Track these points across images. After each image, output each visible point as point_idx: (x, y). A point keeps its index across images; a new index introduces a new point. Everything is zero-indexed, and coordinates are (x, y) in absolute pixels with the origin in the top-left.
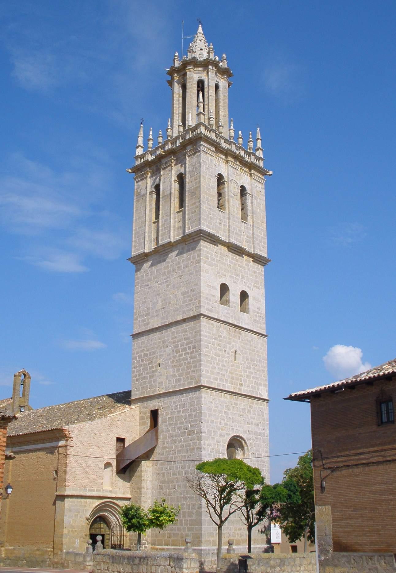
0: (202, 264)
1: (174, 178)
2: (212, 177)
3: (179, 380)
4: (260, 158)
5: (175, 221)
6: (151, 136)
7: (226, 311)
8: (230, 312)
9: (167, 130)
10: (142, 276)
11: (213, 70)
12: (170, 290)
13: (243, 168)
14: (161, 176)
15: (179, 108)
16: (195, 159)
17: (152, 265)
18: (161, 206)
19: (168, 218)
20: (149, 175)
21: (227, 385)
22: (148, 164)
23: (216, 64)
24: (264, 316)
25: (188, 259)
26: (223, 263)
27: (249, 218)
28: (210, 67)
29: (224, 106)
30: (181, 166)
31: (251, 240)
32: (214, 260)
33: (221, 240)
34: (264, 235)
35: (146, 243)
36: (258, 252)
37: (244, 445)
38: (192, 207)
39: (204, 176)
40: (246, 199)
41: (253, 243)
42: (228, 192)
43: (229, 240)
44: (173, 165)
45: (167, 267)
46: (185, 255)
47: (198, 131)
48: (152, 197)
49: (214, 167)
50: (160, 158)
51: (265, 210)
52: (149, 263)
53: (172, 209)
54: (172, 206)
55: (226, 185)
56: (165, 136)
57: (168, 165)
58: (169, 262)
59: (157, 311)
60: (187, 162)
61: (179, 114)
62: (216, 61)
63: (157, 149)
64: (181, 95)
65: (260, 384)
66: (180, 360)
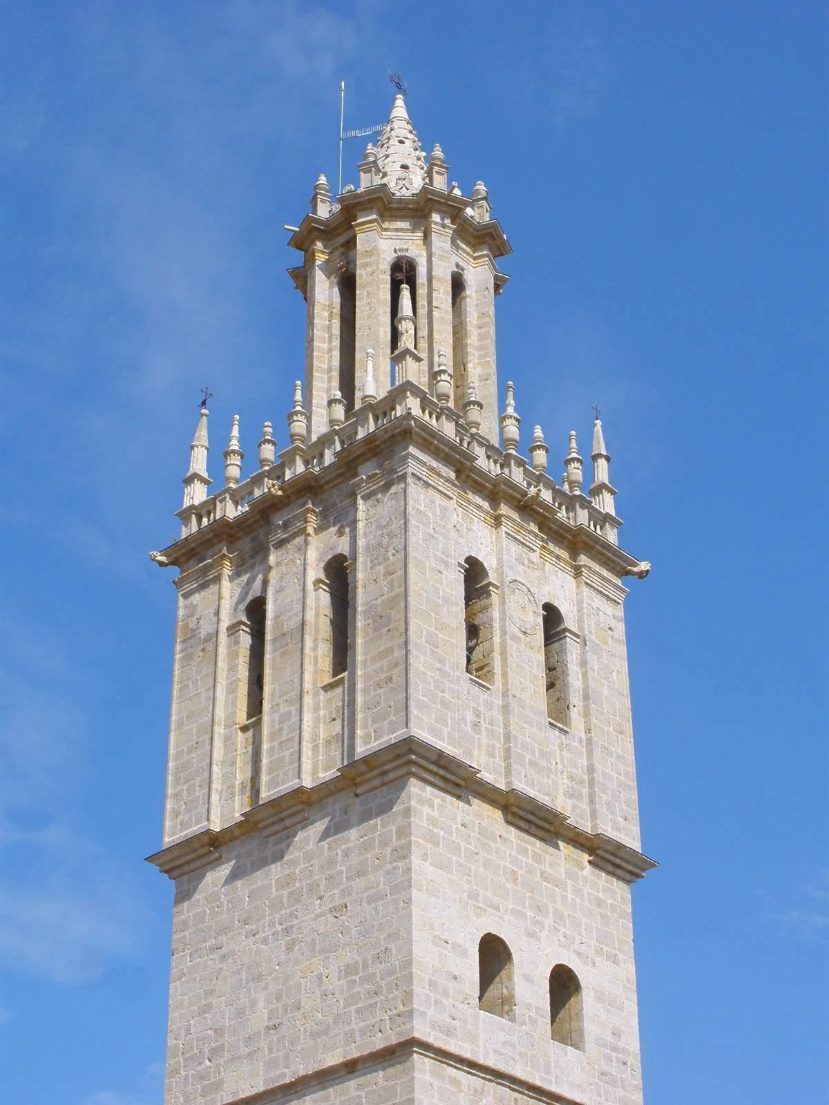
0: (416, 861)
1: (315, 572)
2: (446, 564)
4: (606, 518)
6: (234, 442)
7: (502, 1036)
9: (290, 416)
10: (200, 918)
11: (444, 226)
12: (297, 962)
13: (551, 546)
14: (270, 568)
15: (330, 350)
16: (387, 504)
17: (234, 876)
18: (267, 671)
19: (294, 709)
20: (227, 571)
22: (225, 533)
23: (454, 211)
24: (635, 1061)
25: (366, 847)
27: (575, 714)
28: (436, 217)
29: (481, 348)
30: (340, 533)
31: (585, 791)
32: (456, 849)
33: (481, 783)
35: (215, 798)
38: (378, 665)
40: (563, 651)
41: (592, 801)
42: (503, 620)
44: (310, 530)
45: (288, 880)
46: (353, 833)
47: (399, 411)
48: (237, 642)
49: (453, 534)
50: (265, 511)
51: (626, 689)
52: (224, 870)
53: (308, 677)
55: (495, 598)
56: (284, 437)
57: (292, 530)
58: (294, 863)
60: (361, 515)
61: (330, 370)
62: (455, 199)
63: (257, 480)
64: (337, 310)
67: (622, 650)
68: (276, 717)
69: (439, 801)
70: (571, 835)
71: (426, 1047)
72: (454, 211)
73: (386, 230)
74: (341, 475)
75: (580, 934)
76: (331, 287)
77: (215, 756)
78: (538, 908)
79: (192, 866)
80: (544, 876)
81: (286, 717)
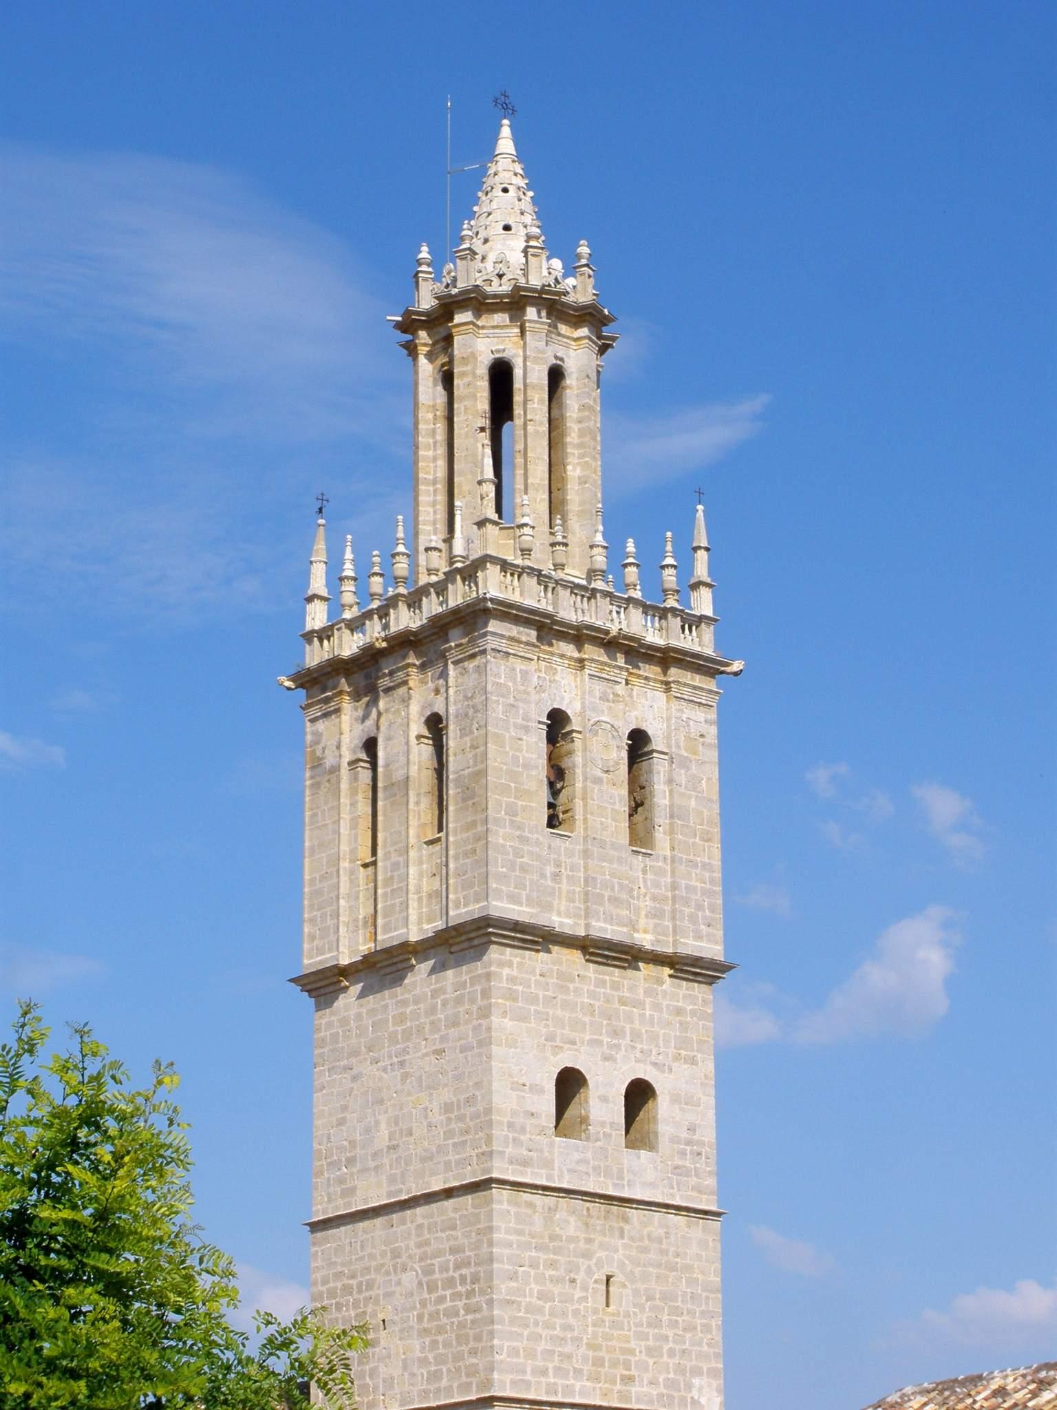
1: (418, 727)
3: (435, 1376)
5: (419, 872)
6: (348, 565)
8: (589, 1155)
12: (409, 1094)
16: (471, 680)
21: (578, 1385)
24: (710, 1151)
26: (566, 1005)
29: (580, 446)
32: (534, 999)
34: (712, 881)
35: (342, 929)
38: (465, 835)
39: (497, 735)
41: (674, 918)
43: (587, 926)
51: (715, 796)
54: (413, 822)
55: (578, 744)
59: (375, 1155)
65: (697, 1372)
66: (437, 1312)
67: (714, 755)
68: (388, 864)
69: (518, 959)
70: (650, 956)
73: (483, 327)
74: (433, 634)
75: (657, 1046)
76: (435, 385)
77: (342, 890)
78: (616, 1033)
79: (327, 990)
80: (622, 1001)
81: (396, 866)
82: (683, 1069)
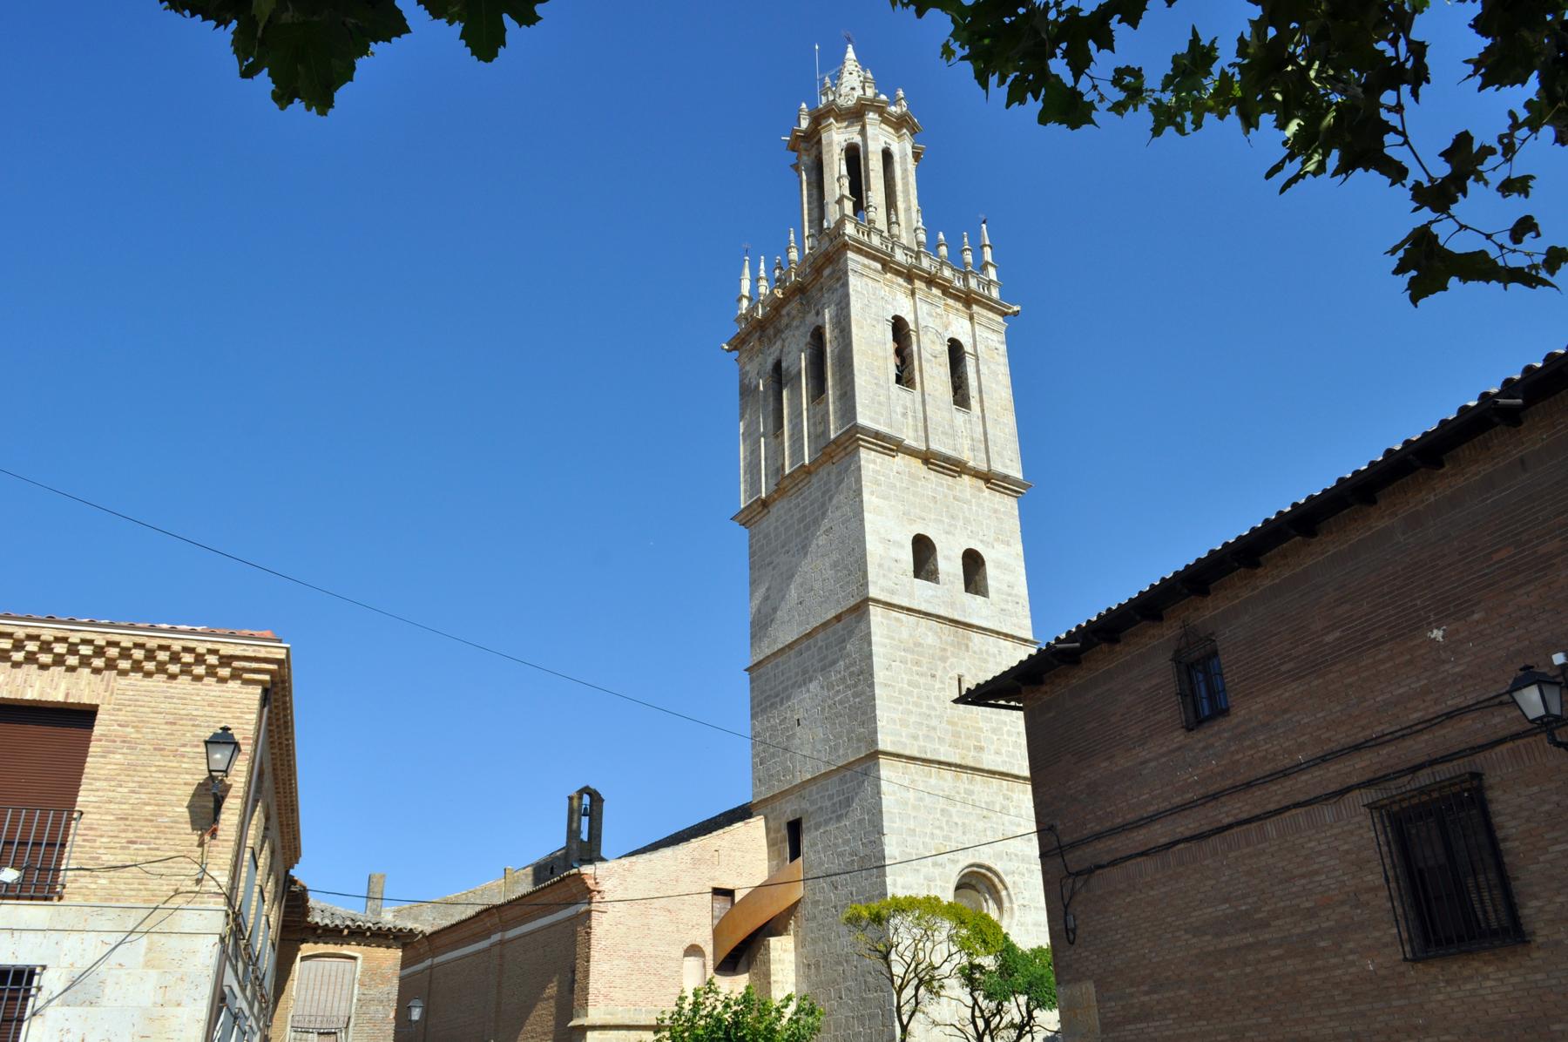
3: (836, 748)
27: (974, 403)
32: (893, 487)
36: (998, 467)
37: (1000, 886)
71: (877, 601)
72: (881, 111)
82: (1000, 547)
